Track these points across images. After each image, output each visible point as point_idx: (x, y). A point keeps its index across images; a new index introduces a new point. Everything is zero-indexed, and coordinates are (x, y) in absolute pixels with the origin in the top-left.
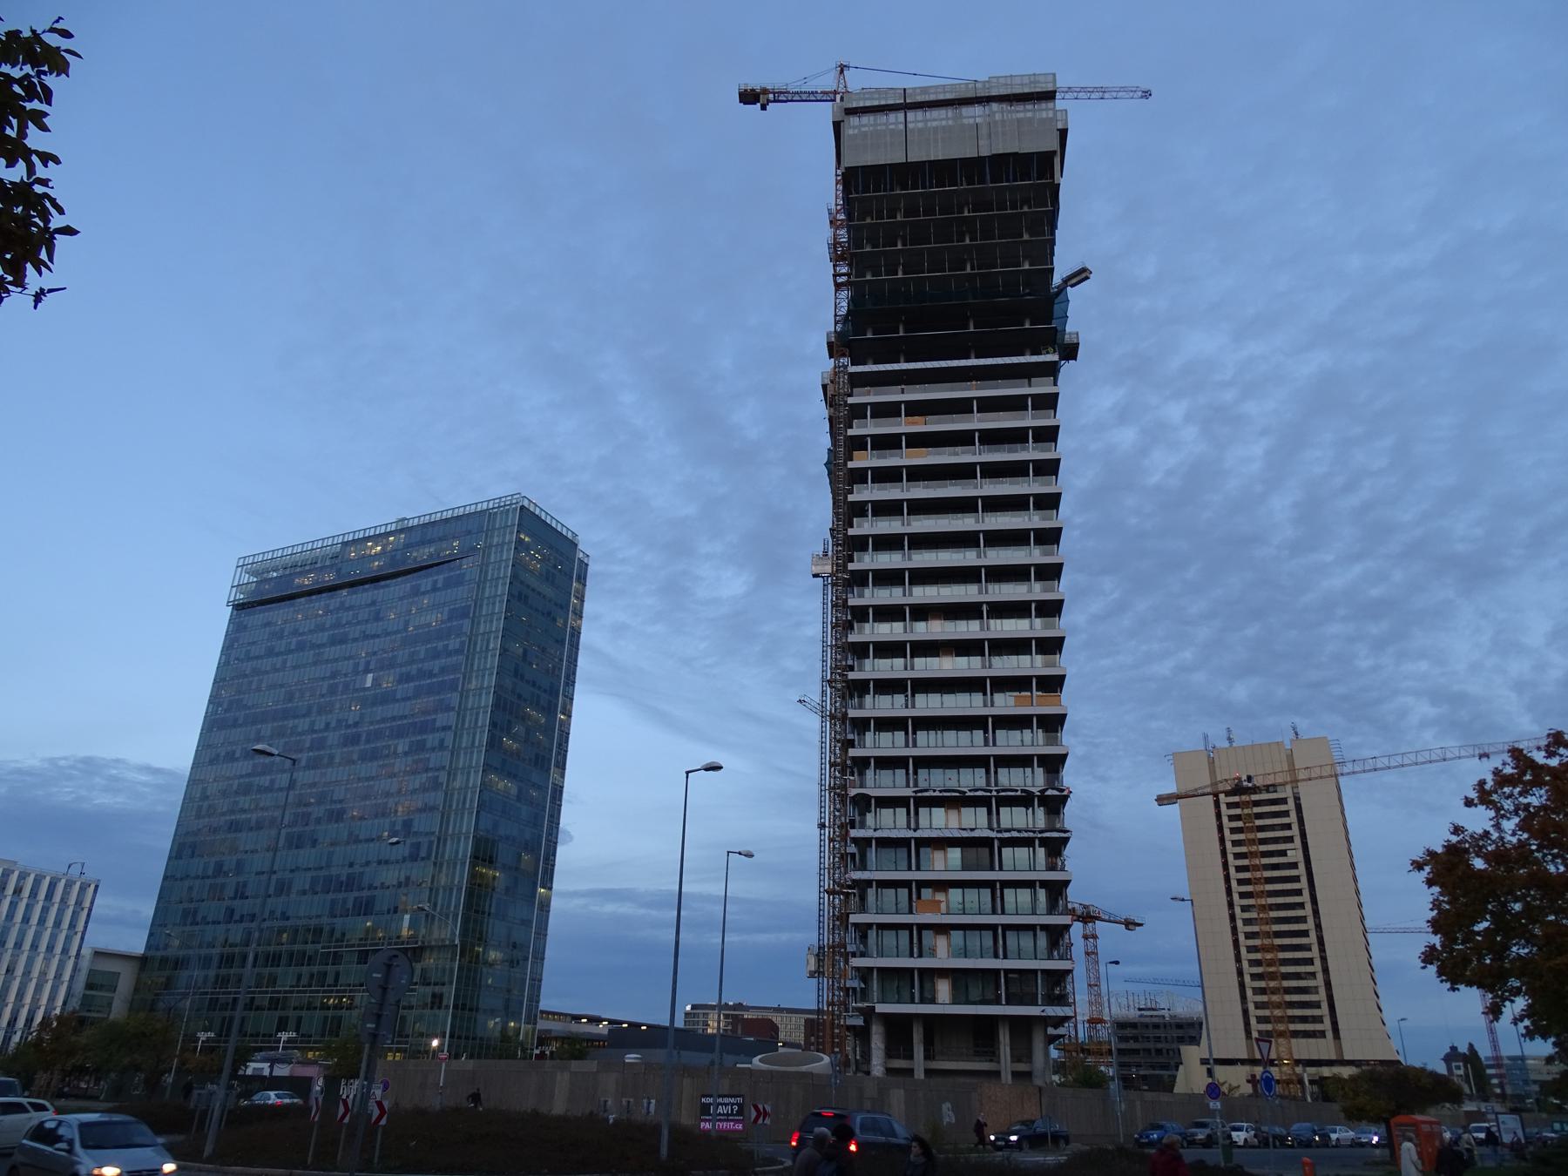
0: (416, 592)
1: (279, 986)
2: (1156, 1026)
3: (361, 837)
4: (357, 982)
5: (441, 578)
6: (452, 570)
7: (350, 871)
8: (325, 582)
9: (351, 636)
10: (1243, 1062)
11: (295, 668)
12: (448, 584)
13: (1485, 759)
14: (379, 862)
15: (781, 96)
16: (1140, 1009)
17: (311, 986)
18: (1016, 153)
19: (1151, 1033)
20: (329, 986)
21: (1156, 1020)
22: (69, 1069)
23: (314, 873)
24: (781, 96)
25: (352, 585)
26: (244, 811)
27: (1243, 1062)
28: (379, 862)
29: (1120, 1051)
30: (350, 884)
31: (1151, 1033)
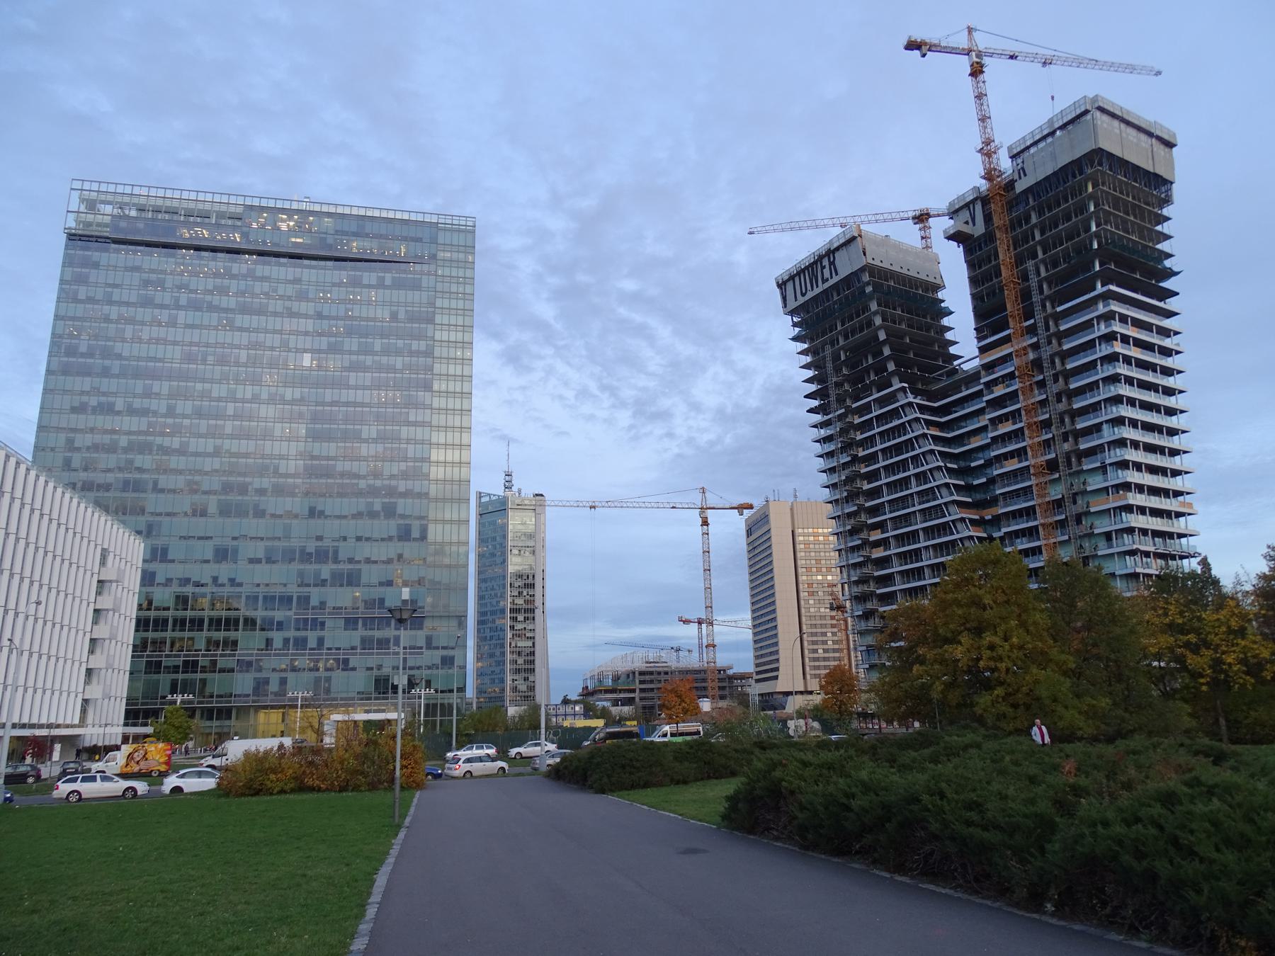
0: (356, 283)
1: (241, 649)
2: (666, 673)
3: (327, 513)
4: (348, 646)
5: (388, 279)
6: (405, 272)
7: (319, 544)
8: (200, 239)
9: (271, 309)
10: (801, 693)
11: (187, 326)
12: (398, 285)
13: (593, 509)
14: (359, 539)
15: (933, 48)
16: (647, 662)
17: (183, 651)
18: (1073, 161)
19: (663, 677)
20: (311, 649)
21: (666, 669)
22: (56, 745)
23: (269, 543)
24: (933, 48)
25: (261, 254)
26: (140, 470)
27: (801, 693)
28: (359, 539)
29: (642, 690)
30: (322, 556)
31: (663, 677)
